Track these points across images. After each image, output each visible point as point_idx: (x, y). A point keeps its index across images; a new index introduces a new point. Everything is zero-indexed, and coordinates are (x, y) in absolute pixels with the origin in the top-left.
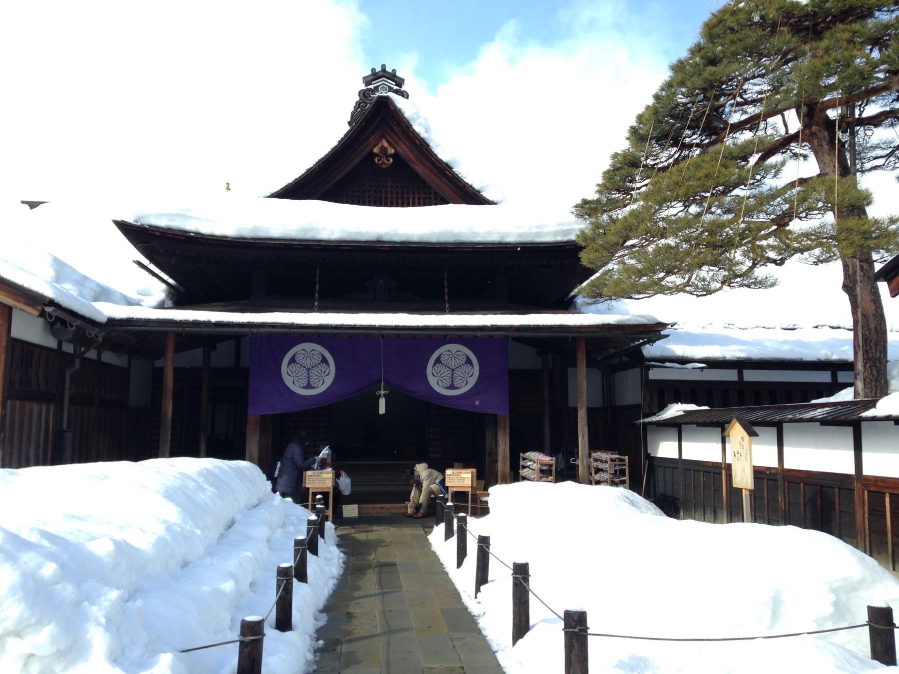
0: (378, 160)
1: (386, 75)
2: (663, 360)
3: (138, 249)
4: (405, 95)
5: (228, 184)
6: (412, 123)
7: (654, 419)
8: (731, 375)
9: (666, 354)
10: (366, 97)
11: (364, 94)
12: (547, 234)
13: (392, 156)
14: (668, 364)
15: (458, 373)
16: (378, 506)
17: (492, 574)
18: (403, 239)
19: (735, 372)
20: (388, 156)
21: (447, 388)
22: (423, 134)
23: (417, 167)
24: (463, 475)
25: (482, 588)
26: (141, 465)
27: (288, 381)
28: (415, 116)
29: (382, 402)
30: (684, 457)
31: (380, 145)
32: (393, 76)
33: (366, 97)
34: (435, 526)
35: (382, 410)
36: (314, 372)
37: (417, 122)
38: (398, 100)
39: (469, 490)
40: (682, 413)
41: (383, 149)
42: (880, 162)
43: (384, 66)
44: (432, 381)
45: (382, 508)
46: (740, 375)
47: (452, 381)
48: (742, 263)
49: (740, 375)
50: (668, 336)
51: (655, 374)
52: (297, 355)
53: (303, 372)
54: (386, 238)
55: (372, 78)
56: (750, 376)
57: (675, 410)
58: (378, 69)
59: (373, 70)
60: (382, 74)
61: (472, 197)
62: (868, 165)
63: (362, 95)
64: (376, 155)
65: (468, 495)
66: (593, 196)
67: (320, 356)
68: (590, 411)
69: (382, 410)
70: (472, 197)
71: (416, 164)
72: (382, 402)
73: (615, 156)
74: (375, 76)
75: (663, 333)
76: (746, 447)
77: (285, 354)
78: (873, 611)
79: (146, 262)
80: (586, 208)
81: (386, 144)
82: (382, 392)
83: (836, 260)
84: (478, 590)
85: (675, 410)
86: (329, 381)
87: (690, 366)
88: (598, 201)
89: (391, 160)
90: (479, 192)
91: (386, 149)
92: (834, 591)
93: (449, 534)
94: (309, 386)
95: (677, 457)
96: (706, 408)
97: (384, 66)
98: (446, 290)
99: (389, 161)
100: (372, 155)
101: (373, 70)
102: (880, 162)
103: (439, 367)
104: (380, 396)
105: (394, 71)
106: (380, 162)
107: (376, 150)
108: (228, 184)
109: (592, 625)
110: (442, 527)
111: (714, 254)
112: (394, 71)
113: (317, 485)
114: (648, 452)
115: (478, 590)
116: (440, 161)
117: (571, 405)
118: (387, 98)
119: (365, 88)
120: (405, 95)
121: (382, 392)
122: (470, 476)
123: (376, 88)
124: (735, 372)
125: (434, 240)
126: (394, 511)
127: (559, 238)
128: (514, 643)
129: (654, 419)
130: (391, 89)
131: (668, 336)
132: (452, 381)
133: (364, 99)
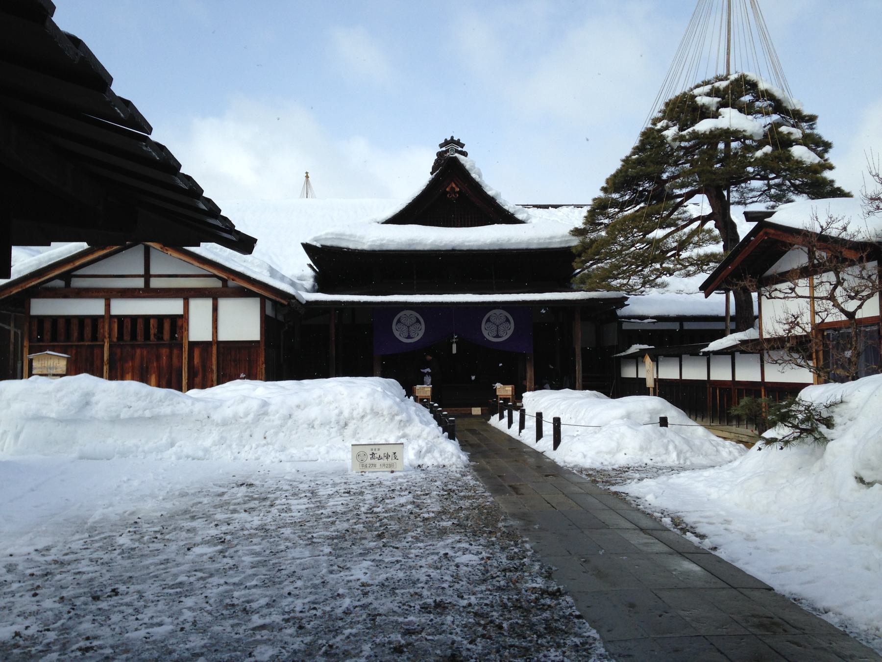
2: (630, 317)
3: (311, 259)
4: (465, 154)
5: (307, 173)
6: (470, 172)
7: (623, 354)
8: (675, 326)
9: (632, 313)
10: (441, 156)
11: (440, 154)
12: (555, 243)
14: (632, 320)
15: (501, 328)
16: (453, 409)
17: (527, 424)
18: (468, 248)
20: (455, 193)
21: (494, 337)
22: (478, 179)
24: (507, 389)
25: (522, 431)
26: (283, 388)
27: (397, 334)
28: (473, 168)
29: (454, 346)
30: (766, 380)
31: (450, 186)
32: (458, 143)
35: (454, 351)
36: (412, 328)
37: (473, 171)
38: (461, 158)
39: (511, 397)
40: (638, 350)
41: (453, 189)
42: (755, 199)
43: (452, 137)
44: (485, 333)
45: (456, 410)
46: (681, 326)
47: (497, 333)
49: (681, 326)
50: (629, 305)
51: (626, 326)
52: (401, 318)
53: (405, 328)
54: (458, 248)
56: (688, 326)
57: (635, 348)
58: (449, 139)
59: (446, 140)
61: (509, 218)
62: (750, 201)
64: (448, 192)
66: (582, 226)
67: (415, 318)
68: (583, 350)
69: (454, 351)
70: (509, 218)
72: (454, 346)
73: (594, 200)
74: (446, 143)
75: (626, 303)
76: (651, 367)
78: (661, 418)
79: (312, 264)
80: (577, 232)
81: (454, 186)
83: (699, 273)
84: (520, 432)
85: (635, 348)
86: (421, 334)
87: (646, 321)
88: (584, 229)
90: (513, 214)
91: (454, 188)
92: (650, 413)
93: (501, 417)
94: (409, 337)
95: (678, 377)
96: (653, 347)
97: (452, 137)
100: (446, 193)
101: (446, 140)
102: (755, 199)
103: (489, 324)
104: (453, 342)
105: (459, 140)
107: (448, 189)
108: (307, 173)
109: (562, 421)
110: (497, 416)
112: (459, 140)
113: (422, 395)
114: (52, 244)
115: (520, 432)
116: (489, 196)
118: (456, 158)
119: (440, 150)
120: (465, 154)
121: (454, 340)
122: (511, 389)
123: (447, 151)
125: (486, 248)
126: (463, 412)
127: (563, 245)
128: (537, 441)
129: (623, 354)
130: (457, 151)
131: (629, 305)
132: (497, 333)
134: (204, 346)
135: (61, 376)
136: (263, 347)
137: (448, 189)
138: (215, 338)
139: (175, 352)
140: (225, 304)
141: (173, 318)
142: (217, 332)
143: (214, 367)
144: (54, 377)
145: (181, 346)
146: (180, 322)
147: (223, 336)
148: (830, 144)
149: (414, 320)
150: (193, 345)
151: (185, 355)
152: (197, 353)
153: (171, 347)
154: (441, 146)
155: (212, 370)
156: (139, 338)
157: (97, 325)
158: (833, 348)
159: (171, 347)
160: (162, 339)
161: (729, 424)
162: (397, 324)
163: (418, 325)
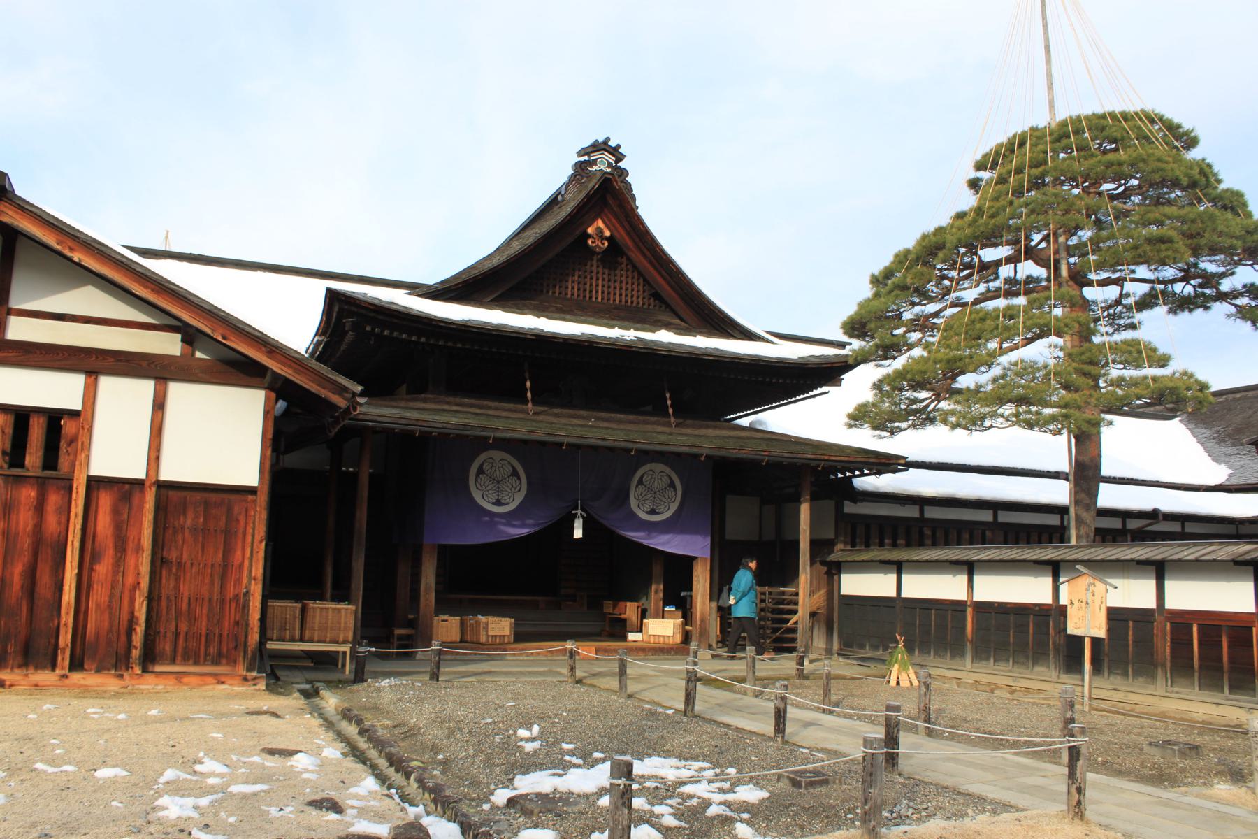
0: (592, 242)
1: (607, 148)
13: (607, 239)
19: (990, 512)
20: (602, 237)
23: (633, 255)
27: (477, 496)
30: (904, 595)
31: (595, 225)
33: (583, 170)
34: (1222, 186)
35: (578, 533)
41: (600, 231)
46: (995, 516)
48: (1198, 234)
49: (995, 516)
55: (591, 150)
56: (932, 513)
60: (603, 146)
63: (578, 166)
64: (589, 236)
65: (797, 543)
69: (578, 533)
71: (632, 251)
77: (473, 460)
81: (600, 223)
82: (579, 512)
89: (606, 244)
95: (893, 594)
98: (669, 402)
99: (603, 244)
104: (575, 516)
106: (594, 245)
107: (590, 230)
111: (1030, 314)
117: (275, 454)
124: (990, 512)
133: (580, 171)
134: (125, 488)
135: (908, 561)
136: (263, 499)
137: (590, 230)
138: (152, 473)
139: (53, 499)
140: (178, 392)
141: (54, 418)
142: (158, 458)
143: (147, 541)
144: (1036, 565)
145: (67, 485)
146: (68, 426)
147: (169, 473)
148: (1170, 357)
149: (666, 480)
150: (96, 484)
151: (78, 509)
152: (105, 501)
153: (42, 484)
154: (580, 154)
155: (139, 548)
156: (29, 460)
157: (273, 451)
158: (194, 530)
159: (42, 484)
160: (21, 465)
161: (996, 664)
162: (477, 476)
163: (670, 491)
